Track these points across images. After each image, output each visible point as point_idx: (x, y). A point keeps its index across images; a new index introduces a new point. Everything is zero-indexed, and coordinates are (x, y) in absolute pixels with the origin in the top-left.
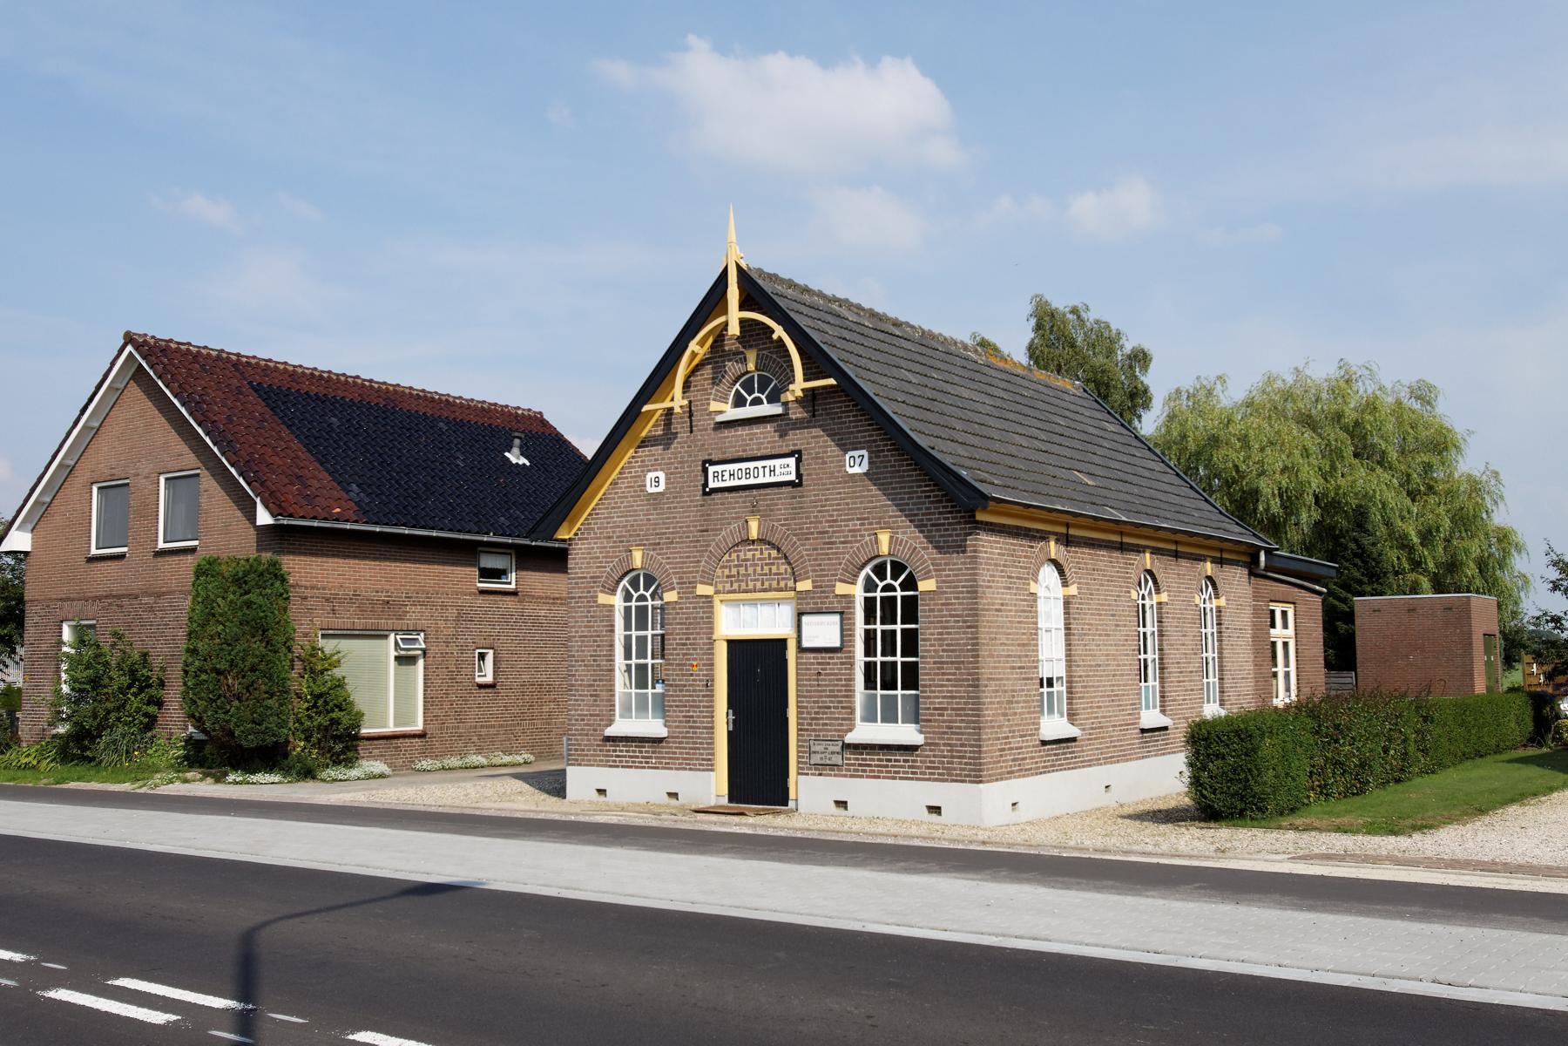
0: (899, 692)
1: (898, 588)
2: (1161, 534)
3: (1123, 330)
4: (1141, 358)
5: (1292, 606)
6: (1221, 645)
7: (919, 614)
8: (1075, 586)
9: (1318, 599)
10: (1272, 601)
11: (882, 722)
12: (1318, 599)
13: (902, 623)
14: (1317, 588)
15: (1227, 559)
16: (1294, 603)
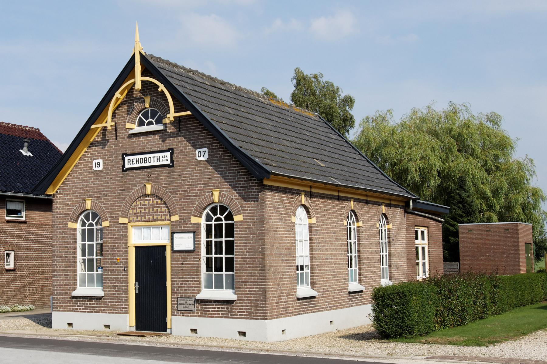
3: (340, 87)
5: (426, 228)
8: (315, 218)
9: (440, 225)
10: (416, 226)
12: (440, 225)
14: (440, 219)
16: (427, 227)
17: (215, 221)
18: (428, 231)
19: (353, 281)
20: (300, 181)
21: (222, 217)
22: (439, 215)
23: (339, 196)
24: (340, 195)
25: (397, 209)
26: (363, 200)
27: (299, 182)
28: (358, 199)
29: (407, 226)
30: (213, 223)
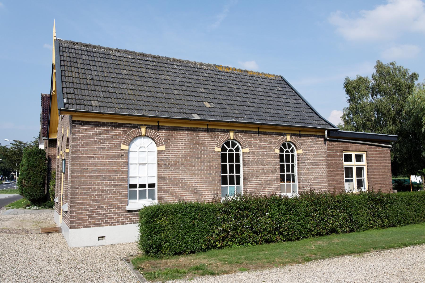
0: (228, 186)
1: (290, 152)
2: (278, 127)
3: (408, 68)
4: (415, 76)
5: (365, 153)
6: (298, 169)
7: (221, 159)
8: (301, 150)
9: (389, 150)
10: (344, 151)
11: (139, 199)
12: (389, 150)
13: (227, 162)
14: (383, 145)
15: (302, 134)
16: (366, 152)
17: (229, 151)
18: (367, 155)
19: (353, 179)
20: (149, 118)
21: (234, 149)
22: (387, 142)
23: (208, 128)
24: (301, 133)
25: (312, 138)
26: (298, 134)
27: (289, 128)
28: (238, 130)
29: (328, 151)
30: (228, 152)
